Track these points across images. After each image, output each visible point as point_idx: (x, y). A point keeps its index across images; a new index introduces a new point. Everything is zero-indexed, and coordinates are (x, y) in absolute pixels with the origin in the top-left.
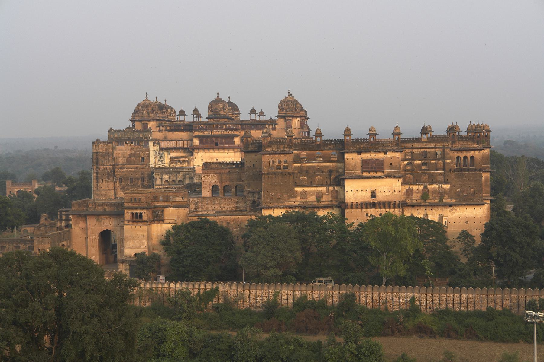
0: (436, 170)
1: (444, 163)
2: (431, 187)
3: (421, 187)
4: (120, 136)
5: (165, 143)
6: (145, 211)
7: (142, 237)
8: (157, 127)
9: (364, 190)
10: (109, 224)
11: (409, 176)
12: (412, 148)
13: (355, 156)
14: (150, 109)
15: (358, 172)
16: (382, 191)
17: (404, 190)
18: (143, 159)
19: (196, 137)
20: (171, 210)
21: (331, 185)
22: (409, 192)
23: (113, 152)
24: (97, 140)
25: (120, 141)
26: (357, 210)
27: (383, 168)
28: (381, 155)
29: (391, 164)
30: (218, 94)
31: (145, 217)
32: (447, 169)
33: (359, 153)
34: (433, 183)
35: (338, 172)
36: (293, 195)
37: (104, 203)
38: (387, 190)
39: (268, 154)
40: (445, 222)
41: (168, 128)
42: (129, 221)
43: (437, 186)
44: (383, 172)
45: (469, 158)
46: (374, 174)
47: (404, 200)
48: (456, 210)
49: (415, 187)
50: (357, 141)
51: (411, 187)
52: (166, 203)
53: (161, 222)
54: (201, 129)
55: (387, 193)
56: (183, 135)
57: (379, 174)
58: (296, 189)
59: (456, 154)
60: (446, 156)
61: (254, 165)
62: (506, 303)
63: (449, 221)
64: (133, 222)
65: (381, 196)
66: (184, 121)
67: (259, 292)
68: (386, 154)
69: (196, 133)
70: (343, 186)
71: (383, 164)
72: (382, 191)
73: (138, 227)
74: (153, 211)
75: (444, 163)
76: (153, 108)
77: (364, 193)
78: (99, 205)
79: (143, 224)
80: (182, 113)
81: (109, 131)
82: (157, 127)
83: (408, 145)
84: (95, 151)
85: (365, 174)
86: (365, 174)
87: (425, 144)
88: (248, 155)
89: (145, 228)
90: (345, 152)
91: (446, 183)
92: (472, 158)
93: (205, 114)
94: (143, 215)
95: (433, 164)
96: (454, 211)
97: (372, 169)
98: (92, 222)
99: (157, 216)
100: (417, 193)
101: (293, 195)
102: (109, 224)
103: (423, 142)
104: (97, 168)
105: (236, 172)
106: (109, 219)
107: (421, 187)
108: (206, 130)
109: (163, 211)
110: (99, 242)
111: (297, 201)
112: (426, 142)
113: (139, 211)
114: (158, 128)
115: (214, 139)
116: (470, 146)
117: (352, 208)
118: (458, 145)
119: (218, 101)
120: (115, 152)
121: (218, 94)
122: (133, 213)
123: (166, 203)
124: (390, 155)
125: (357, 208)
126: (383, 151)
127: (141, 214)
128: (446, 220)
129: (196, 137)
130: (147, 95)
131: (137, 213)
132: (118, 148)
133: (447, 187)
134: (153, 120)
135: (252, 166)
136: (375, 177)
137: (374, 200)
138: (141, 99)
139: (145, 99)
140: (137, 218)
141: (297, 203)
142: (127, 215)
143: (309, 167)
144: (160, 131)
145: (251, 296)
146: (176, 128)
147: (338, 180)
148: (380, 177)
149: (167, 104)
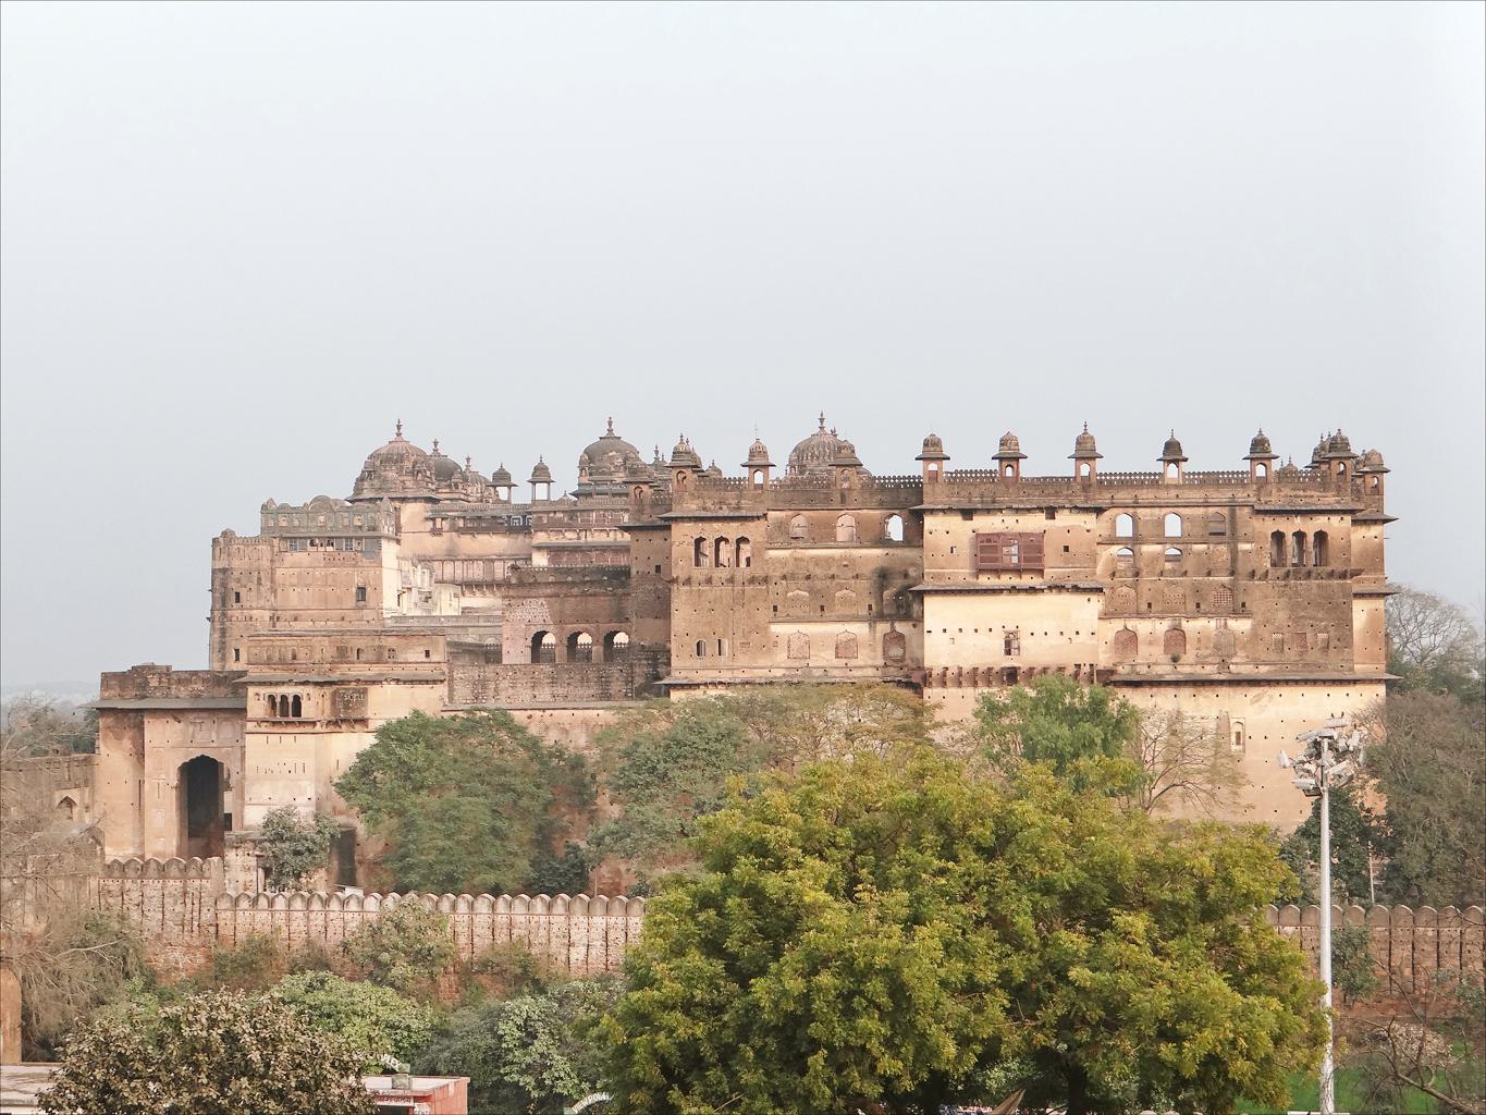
0: (1209, 574)
1: (1234, 553)
2: (1192, 626)
3: (1162, 626)
4: (296, 523)
5: (449, 568)
6: (309, 689)
7: (300, 770)
8: (427, 519)
9: (983, 630)
10: (209, 740)
11: (1123, 594)
12: (1136, 505)
13: (956, 521)
14: (408, 465)
15: (962, 573)
16: (1039, 633)
17: (1110, 636)
18: (362, 590)
19: (539, 548)
20: (390, 689)
21: (881, 617)
22: (1128, 640)
23: (273, 570)
24: (224, 534)
25: (293, 540)
26: (960, 692)
27: (1040, 559)
28: (1035, 522)
29: (1066, 549)
30: (610, 423)
31: (308, 711)
32: (1244, 567)
33: (968, 514)
34: (1199, 611)
35: (906, 575)
36: (768, 646)
37: (195, 673)
38: (1053, 632)
39: (690, 519)
40: (1238, 734)
41: (461, 523)
42: (260, 722)
43: (1213, 623)
44: (1041, 572)
45: (1310, 538)
46: (1015, 581)
47: (1109, 665)
48: (1271, 697)
49: (1143, 627)
50: (959, 479)
51: (1131, 624)
52: (375, 670)
53: (358, 727)
54: (556, 526)
55: (1054, 639)
56: (496, 543)
57: (1027, 580)
58: (776, 629)
59: (1270, 525)
60: (1241, 532)
61: (658, 568)
62: (1402, 953)
63: (1248, 734)
64: (274, 723)
65: (1033, 653)
66: (507, 502)
67: (617, 920)
68: (1051, 512)
69: (541, 538)
70: (918, 621)
71: (1040, 549)
72: (1039, 633)
73: (287, 739)
74: (334, 694)
75: (1234, 553)
76: (415, 462)
77: (983, 639)
78: (179, 682)
79: (301, 729)
80: (502, 478)
81: (264, 507)
82: (427, 519)
83: (1124, 496)
84: (219, 565)
85: (985, 581)
86: (985, 581)
87: (1173, 493)
88: (642, 536)
89: (307, 741)
90: (924, 511)
91: (1241, 611)
92: (1321, 537)
93: (566, 481)
94: (304, 704)
95: (1199, 554)
96: (1265, 700)
97: (1006, 567)
98: (159, 734)
99: (347, 707)
100: (1151, 643)
101: (768, 646)
102: (209, 740)
103: (1168, 487)
104: (224, 615)
105: (605, 595)
106: (208, 723)
107: (1162, 626)
108: (570, 528)
109: (365, 692)
110: (179, 798)
111: (776, 665)
112: (1176, 486)
113: (290, 691)
114: (431, 523)
115: (594, 554)
116: (1315, 500)
117: (944, 684)
118: (1276, 499)
119: (610, 439)
120: (279, 572)
121: (610, 423)
122: (272, 698)
123: (375, 670)
124: (1064, 519)
125: (960, 684)
126: (1040, 509)
127: (297, 699)
128: (1238, 728)
129: (539, 548)
130: (399, 427)
131: (284, 698)
132: (290, 558)
133: (1241, 626)
134: (416, 499)
135: (653, 571)
136: (1013, 590)
137: (1009, 662)
138: (381, 440)
139: (393, 437)
140: (287, 712)
141: (778, 673)
142: (256, 705)
143: (817, 561)
144: (436, 532)
145: (611, 937)
146: (480, 524)
147: (900, 599)
148: (1032, 590)
149: (472, 469)
